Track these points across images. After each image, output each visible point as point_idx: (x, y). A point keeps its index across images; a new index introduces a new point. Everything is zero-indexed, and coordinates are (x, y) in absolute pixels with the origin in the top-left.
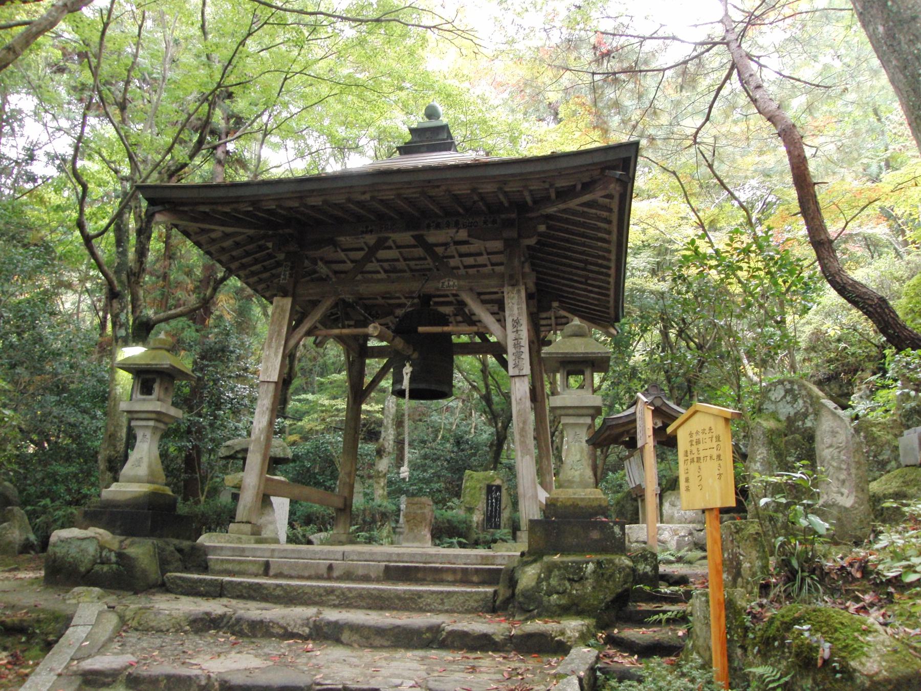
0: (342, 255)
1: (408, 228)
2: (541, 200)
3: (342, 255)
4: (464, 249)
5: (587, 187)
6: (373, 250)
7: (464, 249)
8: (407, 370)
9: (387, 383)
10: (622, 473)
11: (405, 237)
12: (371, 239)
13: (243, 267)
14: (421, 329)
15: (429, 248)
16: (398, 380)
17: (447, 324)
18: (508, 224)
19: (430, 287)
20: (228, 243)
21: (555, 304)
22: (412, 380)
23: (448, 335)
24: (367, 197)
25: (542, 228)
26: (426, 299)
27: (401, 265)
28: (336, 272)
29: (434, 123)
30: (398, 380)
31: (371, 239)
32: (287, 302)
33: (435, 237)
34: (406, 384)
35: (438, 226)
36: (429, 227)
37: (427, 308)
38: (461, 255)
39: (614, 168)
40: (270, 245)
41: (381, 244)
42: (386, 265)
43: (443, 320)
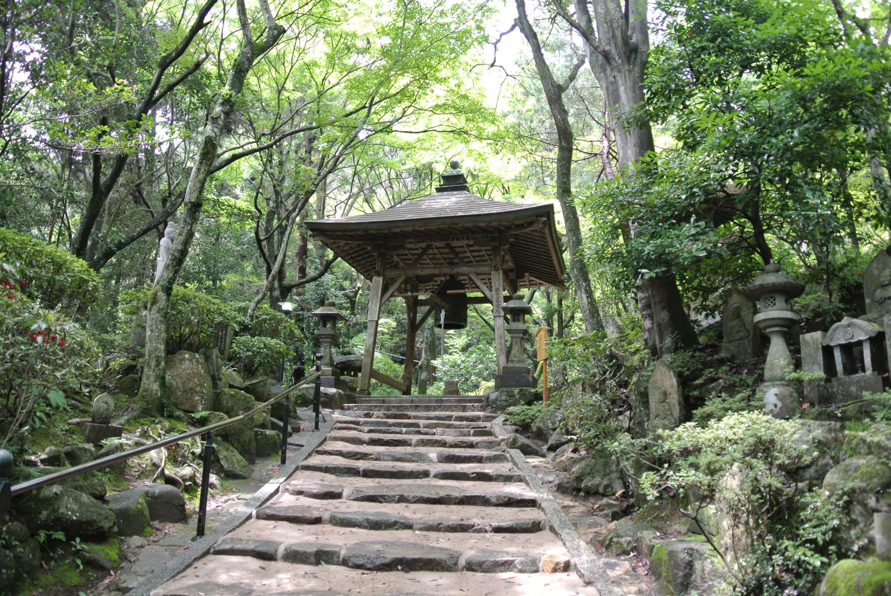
0: (407, 252)
1: (442, 240)
2: (508, 228)
3: (407, 252)
4: (471, 249)
5: (530, 224)
6: (425, 250)
7: (471, 249)
8: (443, 314)
9: (430, 321)
10: (670, 433)
11: (441, 244)
12: (424, 245)
13: (352, 258)
14: (448, 292)
15: (452, 249)
16: (437, 319)
17: (464, 288)
18: (494, 239)
19: (456, 270)
20: (347, 248)
21: (527, 274)
22: (445, 319)
23: (465, 294)
24: (423, 229)
25: (512, 240)
26: (452, 276)
27: (438, 256)
28: (402, 260)
29: (455, 172)
30: (437, 319)
31: (424, 245)
32: (381, 279)
33: (455, 243)
34: (442, 322)
35: (458, 239)
36: (453, 239)
37: (454, 282)
38: (471, 251)
39: (542, 216)
40: (369, 248)
41: (429, 247)
42: (430, 256)
43: (463, 287)
